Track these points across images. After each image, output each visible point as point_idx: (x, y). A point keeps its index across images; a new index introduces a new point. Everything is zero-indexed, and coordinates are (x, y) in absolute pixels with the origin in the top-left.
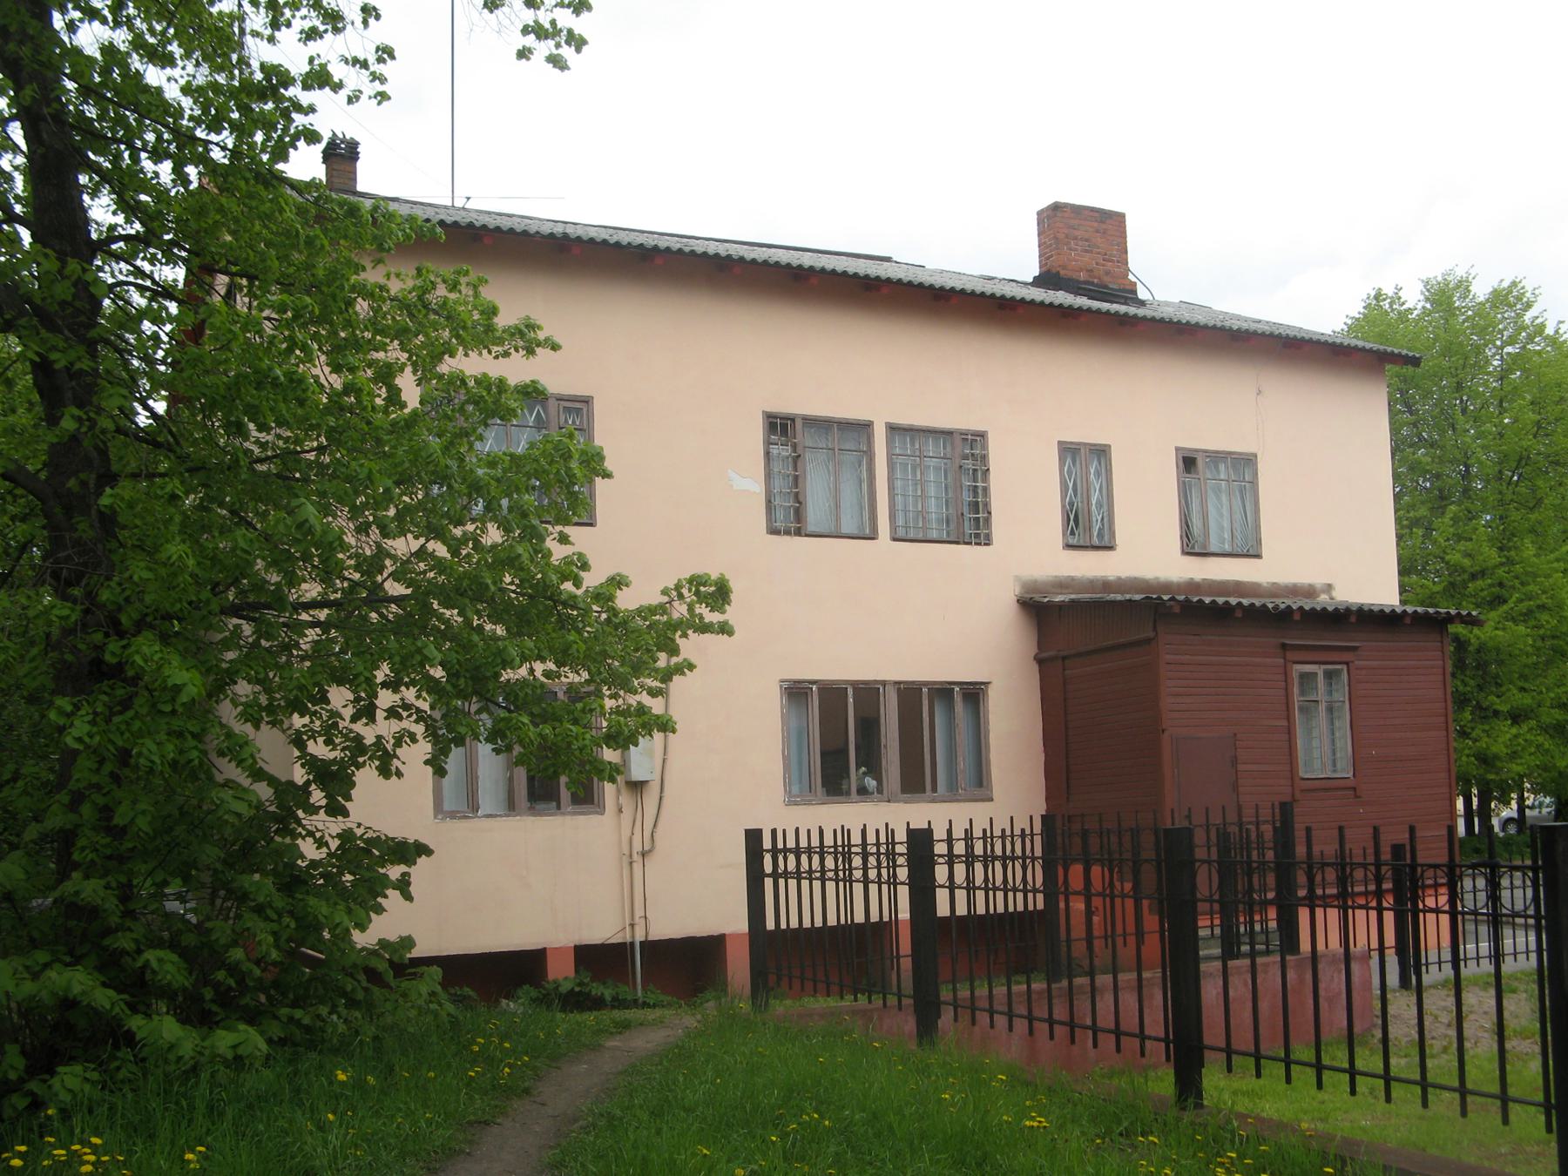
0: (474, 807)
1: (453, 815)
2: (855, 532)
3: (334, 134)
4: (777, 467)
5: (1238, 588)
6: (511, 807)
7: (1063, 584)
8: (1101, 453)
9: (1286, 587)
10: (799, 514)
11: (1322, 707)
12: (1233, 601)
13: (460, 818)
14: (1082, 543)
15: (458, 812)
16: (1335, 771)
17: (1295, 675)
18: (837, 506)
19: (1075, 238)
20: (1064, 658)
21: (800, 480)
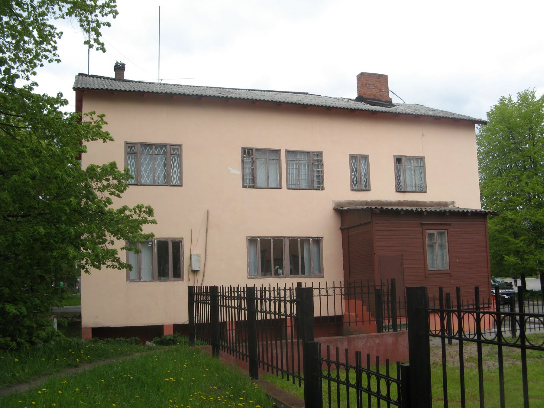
0: (140, 278)
1: (133, 281)
2: (275, 186)
3: (117, 62)
4: (247, 165)
5: (417, 204)
6: (153, 279)
7: (350, 203)
8: (366, 158)
9: (436, 203)
10: (254, 180)
11: (437, 245)
12: (400, 208)
13: (135, 282)
14: (358, 189)
15: (135, 280)
16: (443, 268)
17: (426, 234)
18: (268, 178)
19: (369, 84)
20: (348, 228)
21: (254, 170)
